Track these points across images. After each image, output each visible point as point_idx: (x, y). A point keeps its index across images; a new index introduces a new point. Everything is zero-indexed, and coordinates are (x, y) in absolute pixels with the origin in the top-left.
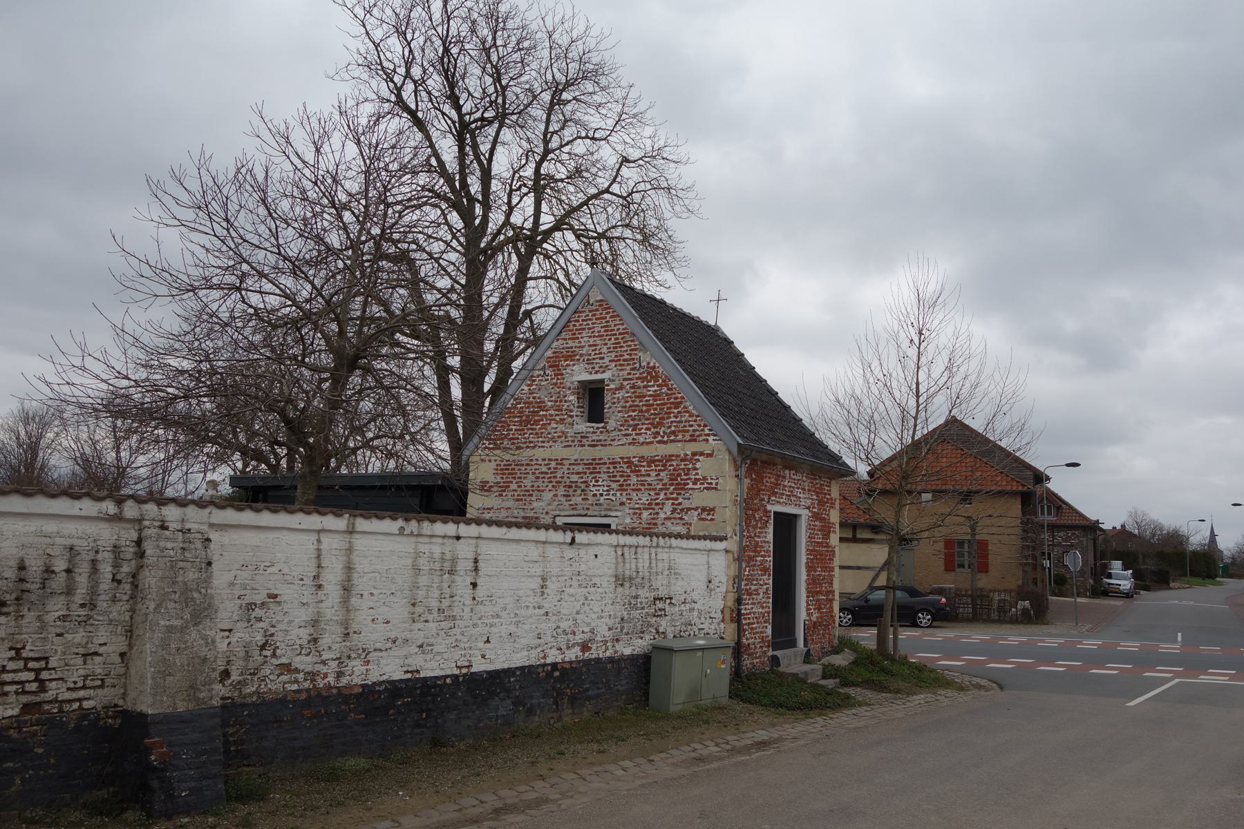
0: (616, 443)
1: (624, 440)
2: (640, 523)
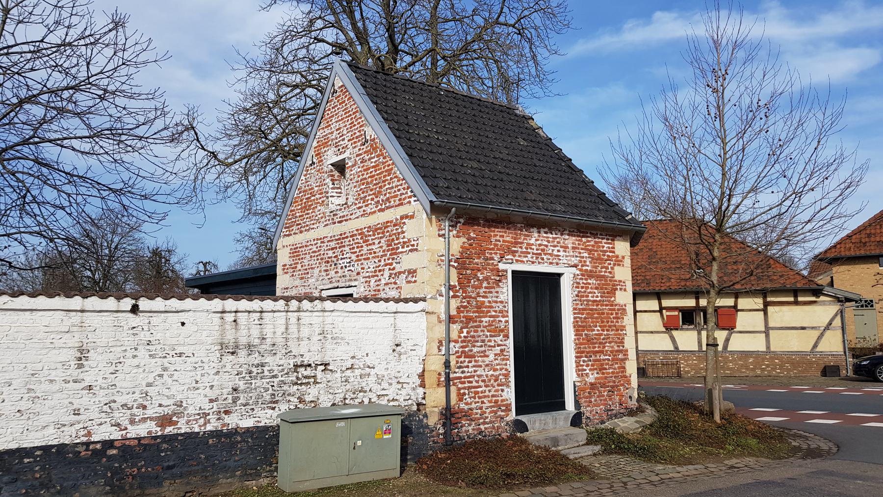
0: (353, 216)
1: (359, 214)
2: (370, 291)
